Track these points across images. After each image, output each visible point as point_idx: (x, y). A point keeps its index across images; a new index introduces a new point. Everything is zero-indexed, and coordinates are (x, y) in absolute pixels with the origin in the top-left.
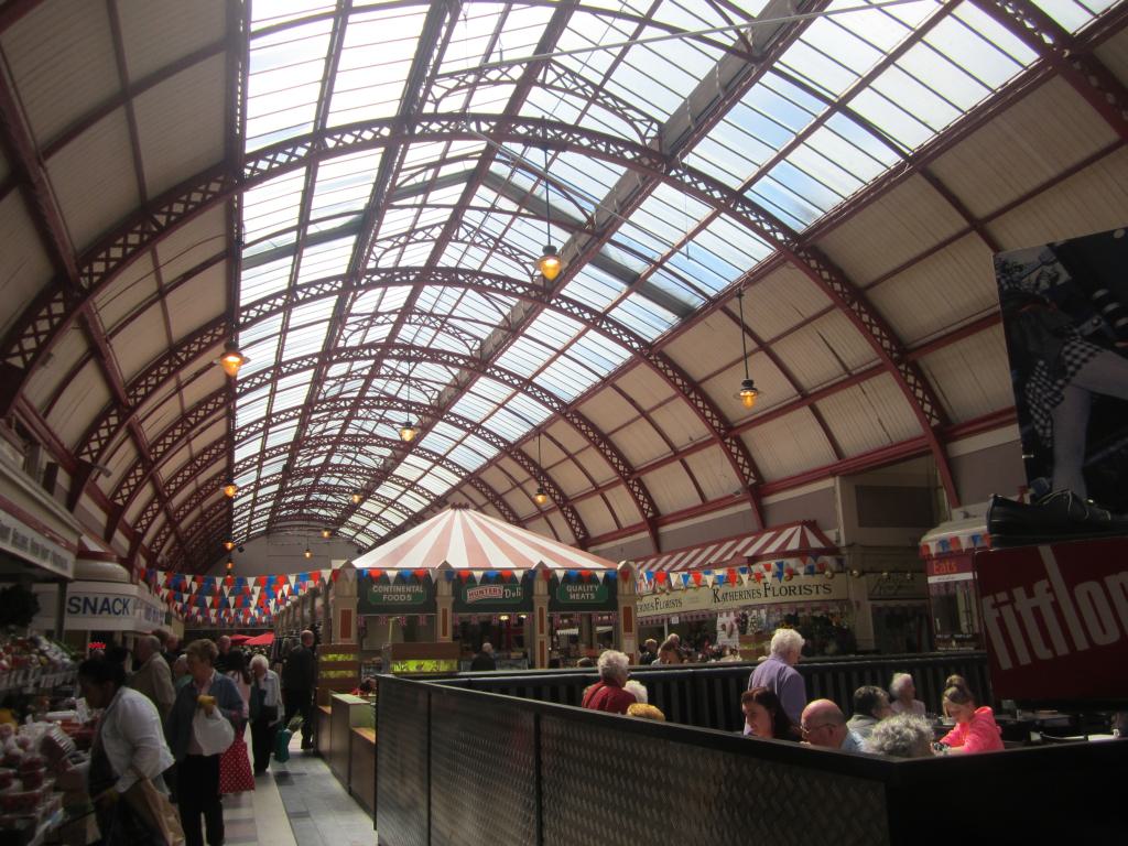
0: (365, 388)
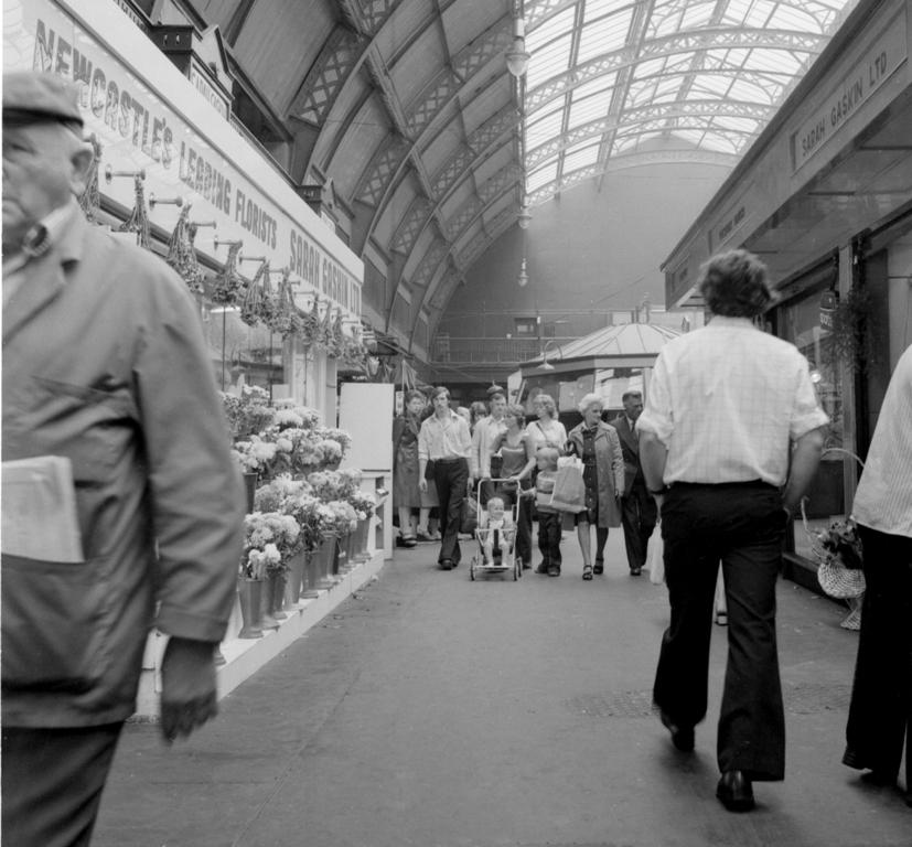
0: (684, 89)
